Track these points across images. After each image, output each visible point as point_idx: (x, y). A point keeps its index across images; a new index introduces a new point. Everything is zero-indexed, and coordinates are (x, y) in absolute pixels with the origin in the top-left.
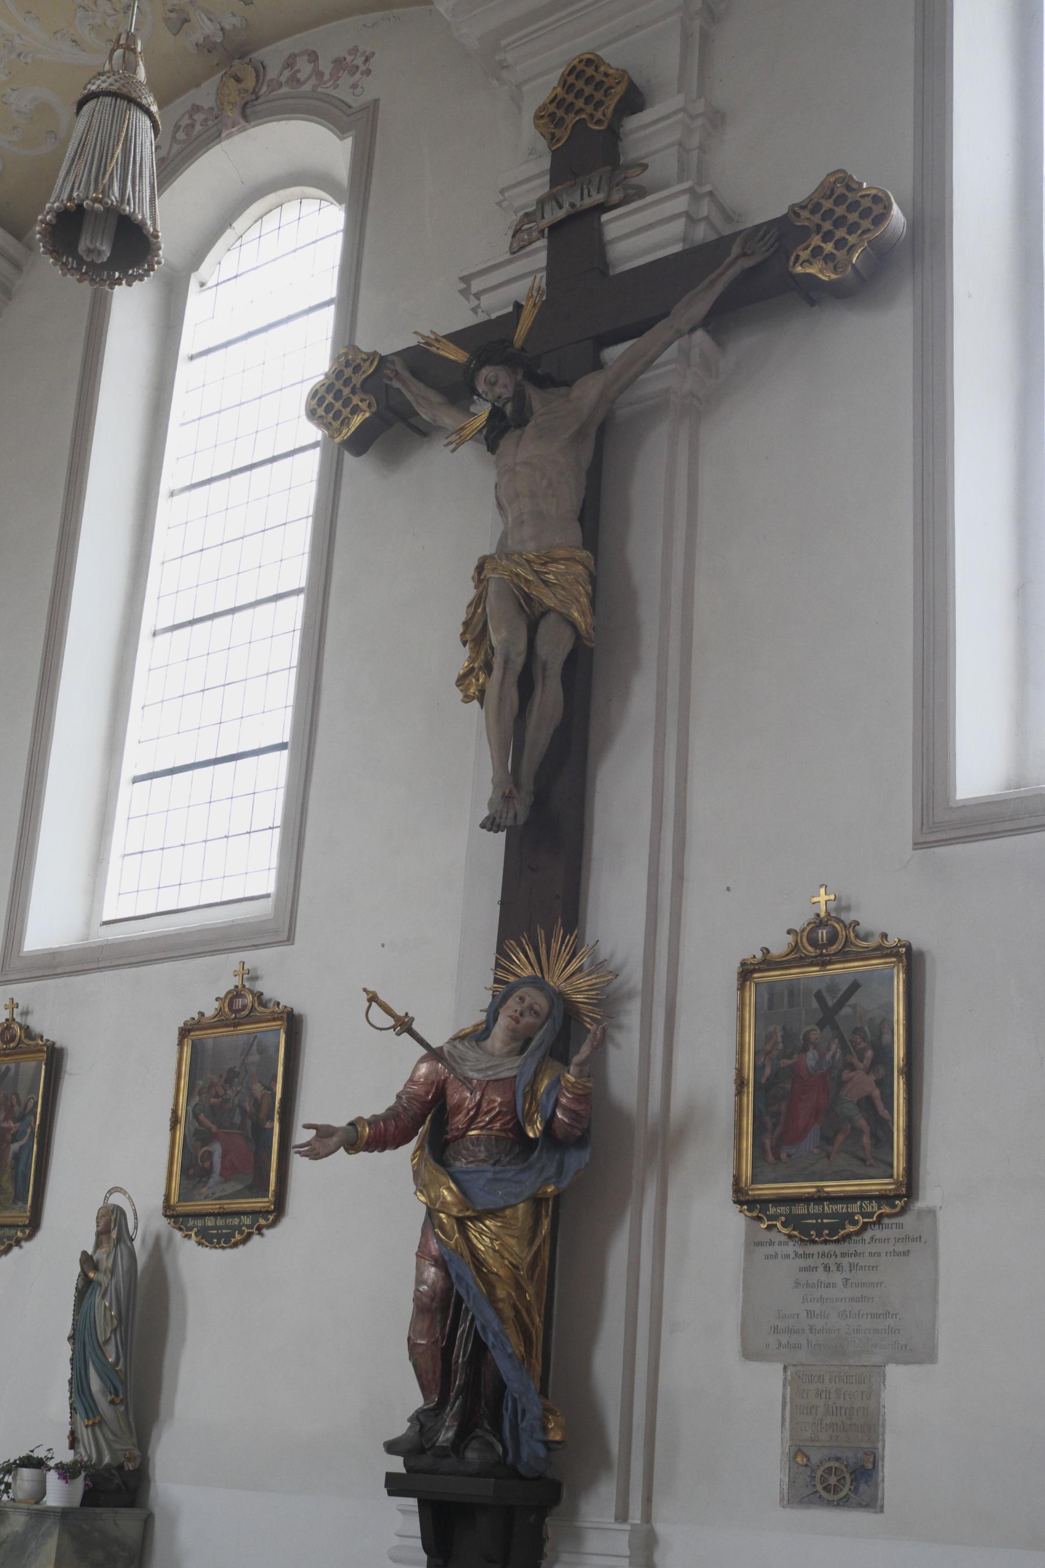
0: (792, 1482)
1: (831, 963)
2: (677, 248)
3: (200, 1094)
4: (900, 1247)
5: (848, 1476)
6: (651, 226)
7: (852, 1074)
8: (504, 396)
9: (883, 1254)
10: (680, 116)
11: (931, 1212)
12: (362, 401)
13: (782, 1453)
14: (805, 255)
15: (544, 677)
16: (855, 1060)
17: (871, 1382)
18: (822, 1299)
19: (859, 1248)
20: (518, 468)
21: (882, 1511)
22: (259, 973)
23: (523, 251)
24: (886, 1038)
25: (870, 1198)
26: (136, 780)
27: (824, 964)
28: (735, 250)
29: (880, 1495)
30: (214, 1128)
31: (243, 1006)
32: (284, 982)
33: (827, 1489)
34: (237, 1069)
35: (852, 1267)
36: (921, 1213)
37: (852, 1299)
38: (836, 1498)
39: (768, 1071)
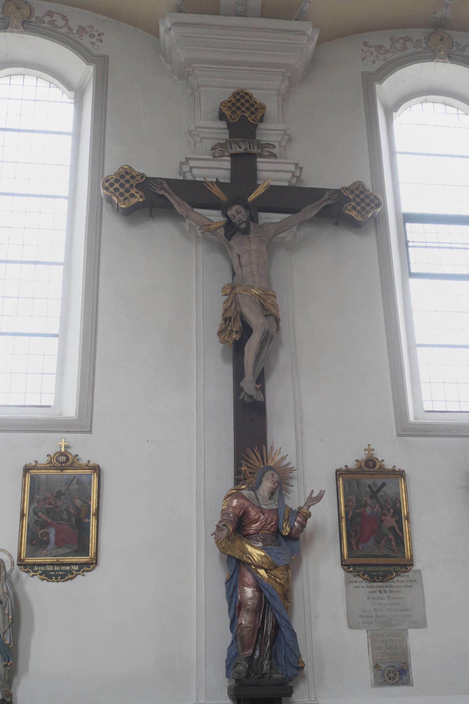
0: (375, 677)
2: (286, 184)
3: (38, 502)
4: (409, 584)
5: (397, 673)
6: (277, 171)
7: (386, 518)
8: (243, 220)
9: (402, 587)
10: (283, 132)
11: (419, 571)
12: (136, 193)
13: (370, 666)
14: (349, 207)
15: (270, 342)
16: (387, 512)
17: (402, 637)
18: (380, 604)
19: (393, 584)
20: (252, 252)
21: (412, 685)
23: (219, 158)
24: (398, 505)
25: (398, 565)
28: (326, 196)
29: (411, 679)
30: (49, 520)
31: (64, 460)
32: (86, 449)
33: (390, 679)
34: (63, 492)
35: (390, 591)
36: (415, 571)
37: (392, 604)
38: (394, 682)
39: (351, 514)
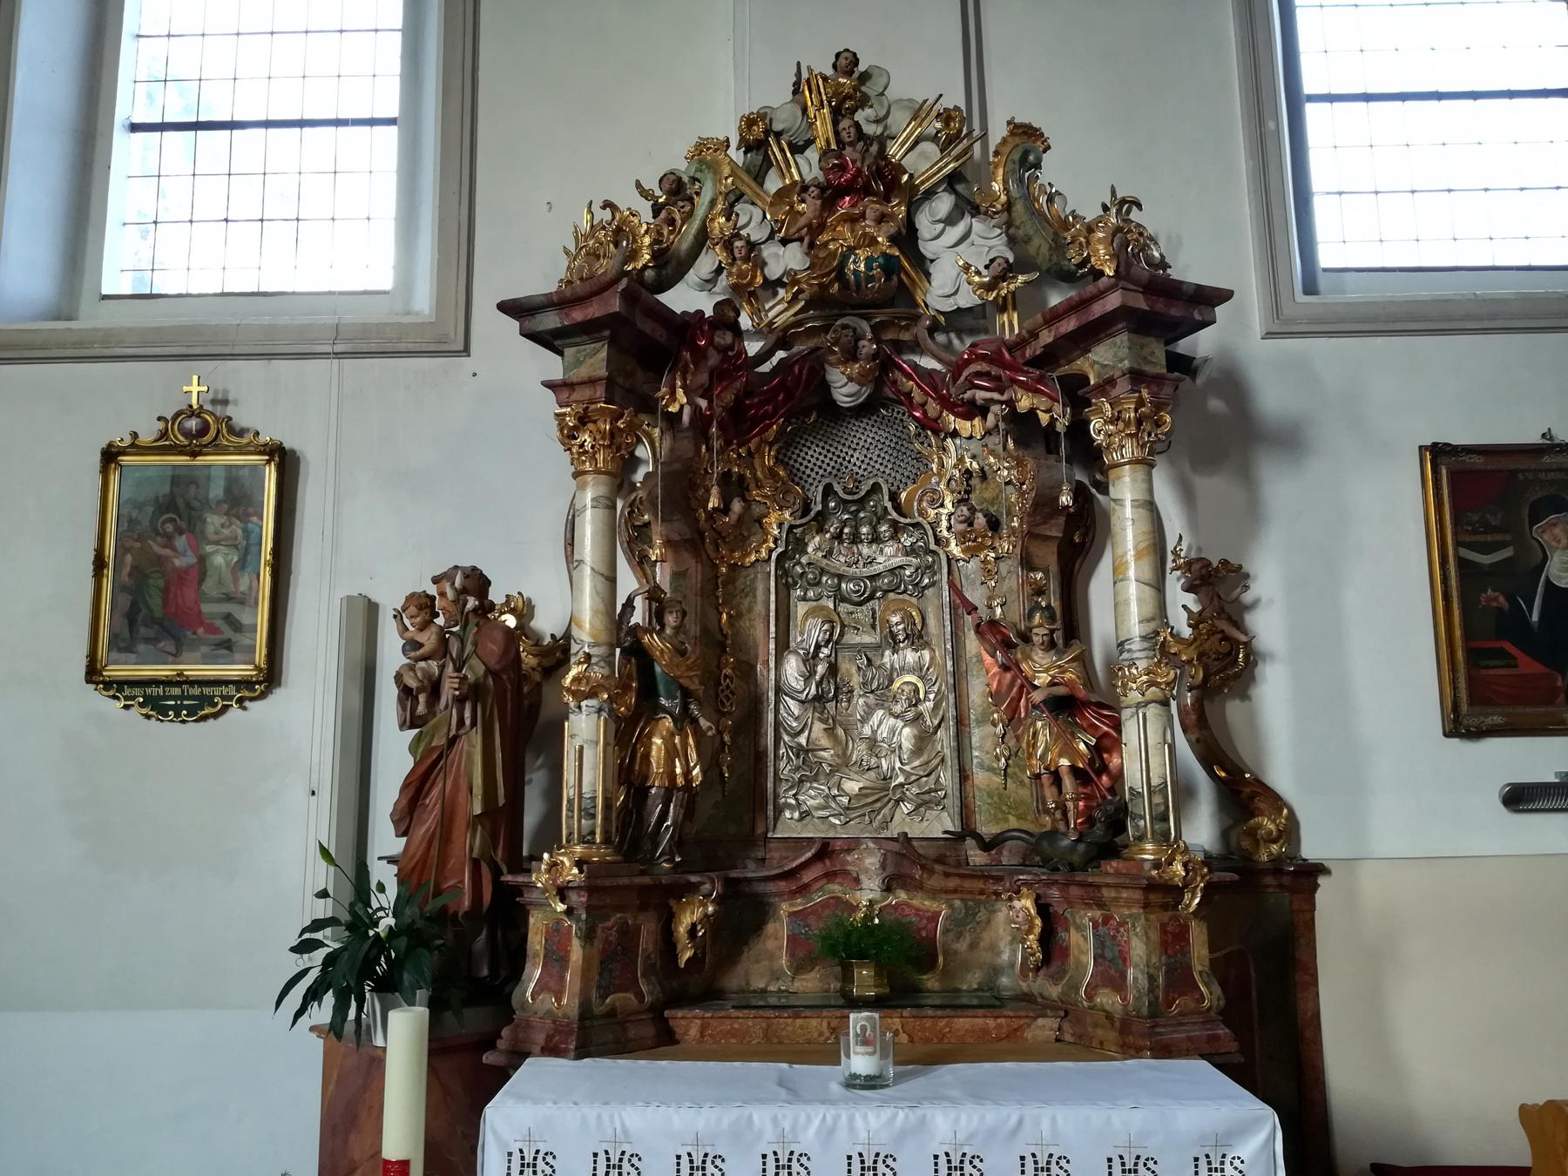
1: (200, 454)
22: (231, 398)
25: (226, 683)
26: (135, 128)
27: (194, 454)
